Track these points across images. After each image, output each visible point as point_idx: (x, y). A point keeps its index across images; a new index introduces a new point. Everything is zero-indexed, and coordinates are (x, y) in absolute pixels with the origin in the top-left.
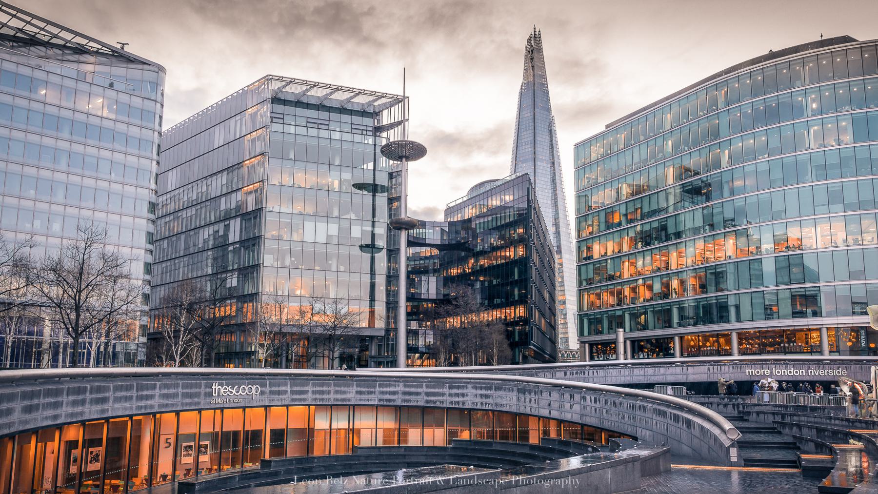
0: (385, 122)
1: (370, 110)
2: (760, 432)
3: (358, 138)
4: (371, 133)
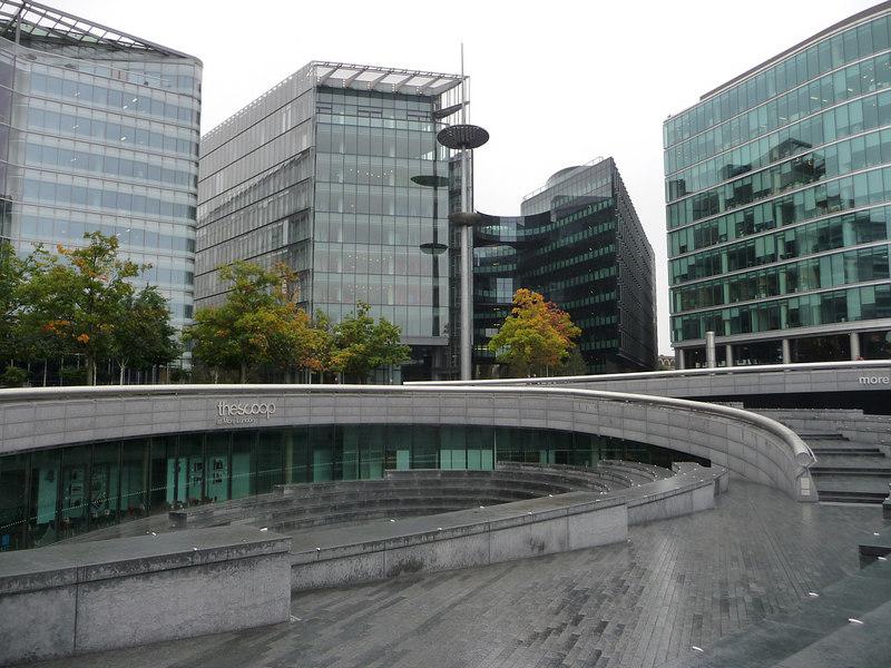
0: (444, 106)
1: (428, 93)
2: (856, 455)
3: (414, 126)
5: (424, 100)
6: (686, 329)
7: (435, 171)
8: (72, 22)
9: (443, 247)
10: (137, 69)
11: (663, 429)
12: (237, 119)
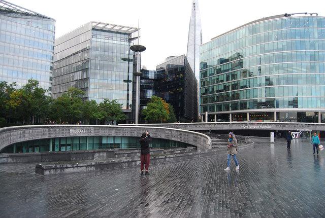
3: (123, 43)
5: (128, 35)
8: (14, 7)
9: (130, 81)
10: (35, 23)
12: (65, 36)
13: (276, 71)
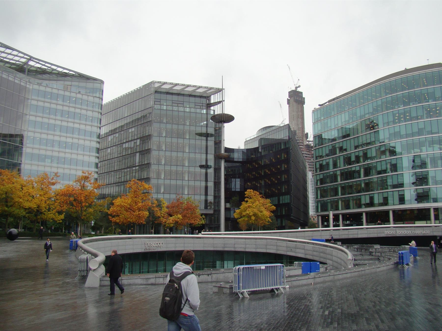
0: (212, 101)
1: (205, 95)
3: (198, 111)
4: (205, 107)
5: (203, 98)
6: (323, 206)
7: (207, 131)
11: (311, 252)
13: (430, 147)
